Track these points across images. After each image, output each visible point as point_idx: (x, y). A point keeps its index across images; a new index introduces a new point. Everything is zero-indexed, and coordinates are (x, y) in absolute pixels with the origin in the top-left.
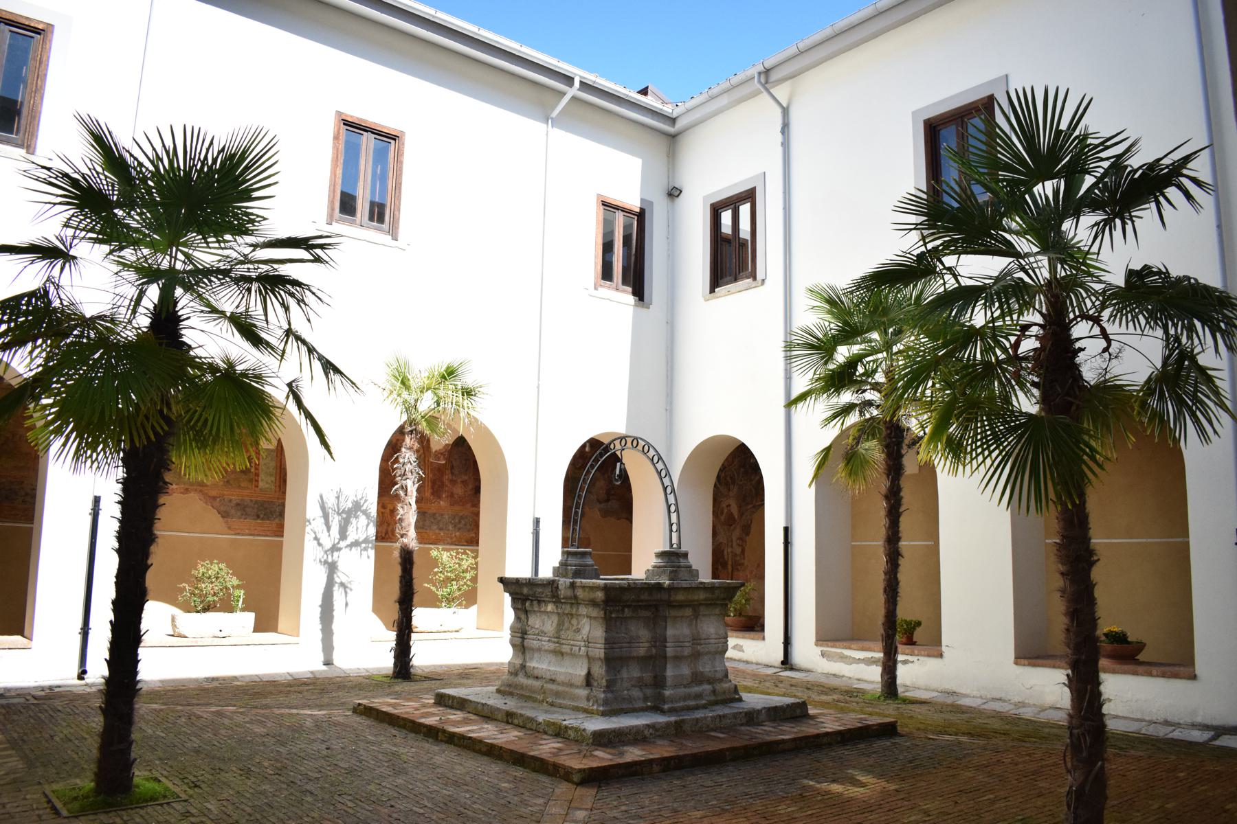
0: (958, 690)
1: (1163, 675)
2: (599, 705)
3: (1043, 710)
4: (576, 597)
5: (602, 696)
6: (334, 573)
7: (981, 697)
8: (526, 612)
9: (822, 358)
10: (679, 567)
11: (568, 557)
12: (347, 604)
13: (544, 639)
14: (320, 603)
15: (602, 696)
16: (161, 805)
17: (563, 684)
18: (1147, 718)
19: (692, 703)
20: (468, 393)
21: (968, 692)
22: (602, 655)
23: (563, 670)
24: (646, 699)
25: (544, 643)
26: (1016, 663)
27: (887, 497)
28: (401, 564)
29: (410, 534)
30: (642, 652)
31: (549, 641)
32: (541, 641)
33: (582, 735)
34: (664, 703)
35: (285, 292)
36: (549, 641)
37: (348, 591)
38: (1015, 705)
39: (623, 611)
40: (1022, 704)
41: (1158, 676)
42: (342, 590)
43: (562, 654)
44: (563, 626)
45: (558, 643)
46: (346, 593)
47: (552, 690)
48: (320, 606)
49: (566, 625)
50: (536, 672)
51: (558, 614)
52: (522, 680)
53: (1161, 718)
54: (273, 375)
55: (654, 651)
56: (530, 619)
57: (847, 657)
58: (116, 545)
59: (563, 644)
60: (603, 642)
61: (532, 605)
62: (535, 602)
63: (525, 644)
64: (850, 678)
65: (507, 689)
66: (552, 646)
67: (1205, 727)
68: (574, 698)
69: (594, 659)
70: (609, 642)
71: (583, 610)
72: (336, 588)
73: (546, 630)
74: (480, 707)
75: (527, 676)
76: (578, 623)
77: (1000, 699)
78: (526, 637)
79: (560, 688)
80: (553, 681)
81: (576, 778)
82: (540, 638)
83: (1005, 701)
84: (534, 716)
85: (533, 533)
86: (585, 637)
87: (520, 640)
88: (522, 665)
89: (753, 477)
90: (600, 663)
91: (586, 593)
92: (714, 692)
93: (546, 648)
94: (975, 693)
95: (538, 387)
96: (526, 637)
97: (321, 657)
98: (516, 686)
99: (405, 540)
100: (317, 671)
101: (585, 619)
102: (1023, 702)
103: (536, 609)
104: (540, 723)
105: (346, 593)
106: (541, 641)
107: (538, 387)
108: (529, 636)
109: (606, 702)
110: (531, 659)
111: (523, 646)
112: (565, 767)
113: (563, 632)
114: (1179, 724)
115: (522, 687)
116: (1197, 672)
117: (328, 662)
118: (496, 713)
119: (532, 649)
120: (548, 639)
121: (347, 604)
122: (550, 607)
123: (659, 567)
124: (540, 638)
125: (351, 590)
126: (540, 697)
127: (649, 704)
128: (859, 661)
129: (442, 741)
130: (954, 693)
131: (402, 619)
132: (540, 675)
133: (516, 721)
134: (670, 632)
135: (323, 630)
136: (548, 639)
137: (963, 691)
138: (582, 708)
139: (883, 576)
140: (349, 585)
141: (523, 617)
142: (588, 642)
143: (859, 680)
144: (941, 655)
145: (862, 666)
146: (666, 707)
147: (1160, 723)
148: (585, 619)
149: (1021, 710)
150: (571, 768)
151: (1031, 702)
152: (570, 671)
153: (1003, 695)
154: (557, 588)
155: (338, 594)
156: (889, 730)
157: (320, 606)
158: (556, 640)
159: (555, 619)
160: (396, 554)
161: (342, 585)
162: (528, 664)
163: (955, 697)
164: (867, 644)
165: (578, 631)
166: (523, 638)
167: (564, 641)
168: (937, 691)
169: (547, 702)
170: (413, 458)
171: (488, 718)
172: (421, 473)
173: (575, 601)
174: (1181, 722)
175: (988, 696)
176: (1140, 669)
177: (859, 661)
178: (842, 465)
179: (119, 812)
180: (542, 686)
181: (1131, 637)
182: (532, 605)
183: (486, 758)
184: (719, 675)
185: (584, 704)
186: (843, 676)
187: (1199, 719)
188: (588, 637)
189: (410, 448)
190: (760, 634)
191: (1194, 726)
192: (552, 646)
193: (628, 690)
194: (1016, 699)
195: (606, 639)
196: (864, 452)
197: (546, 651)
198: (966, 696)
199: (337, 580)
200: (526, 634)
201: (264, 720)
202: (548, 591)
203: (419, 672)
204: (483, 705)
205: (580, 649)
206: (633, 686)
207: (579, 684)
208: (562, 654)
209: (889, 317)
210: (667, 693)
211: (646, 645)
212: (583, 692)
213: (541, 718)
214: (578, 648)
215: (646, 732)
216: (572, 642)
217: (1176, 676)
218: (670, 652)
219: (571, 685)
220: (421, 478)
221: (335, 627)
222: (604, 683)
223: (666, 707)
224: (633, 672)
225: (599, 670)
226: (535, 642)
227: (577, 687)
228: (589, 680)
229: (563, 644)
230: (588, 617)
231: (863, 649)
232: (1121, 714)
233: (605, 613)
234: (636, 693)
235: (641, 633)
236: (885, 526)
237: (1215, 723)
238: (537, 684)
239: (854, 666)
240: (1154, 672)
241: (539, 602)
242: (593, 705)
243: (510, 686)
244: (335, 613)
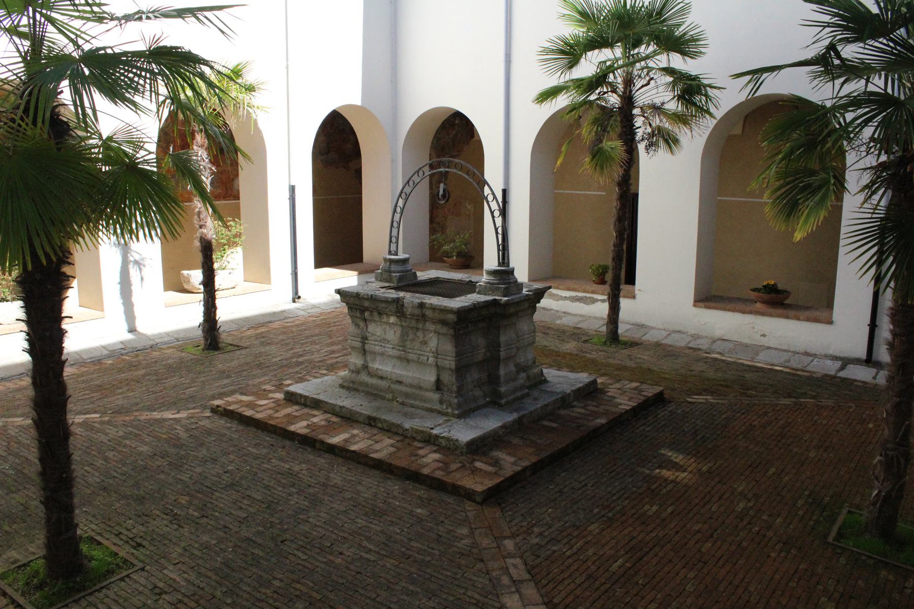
0: (646, 323)
1: (808, 320)
2: (453, 409)
3: (714, 341)
4: (424, 316)
5: (456, 401)
6: (128, 252)
7: (664, 329)
8: (365, 320)
9: (570, 62)
10: (510, 283)
11: (390, 264)
12: (142, 279)
13: (388, 346)
14: (118, 280)
15: (456, 401)
16: (122, 579)
17: (411, 386)
18: (792, 350)
19: (519, 394)
20: (250, 89)
21: (654, 325)
22: (453, 367)
23: (410, 374)
24: (485, 396)
25: (389, 350)
26: (695, 306)
27: (619, 184)
28: (202, 251)
29: (208, 224)
30: (480, 357)
31: (393, 348)
32: (384, 347)
33: (454, 444)
34: (501, 398)
35: (194, 75)
36: (393, 348)
37: (142, 267)
38: (692, 337)
39: (467, 326)
40: (696, 337)
41: (804, 320)
42: (136, 267)
43: (408, 361)
44: (408, 336)
45: (403, 351)
46: (140, 269)
47: (401, 391)
48: (119, 283)
49: (411, 336)
50: (380, 373)
51: (402, 326)
52: (364, 377)
53: (802, 350)
54: (148, 140)
55: (488, 354)
56: (369, 327)
57: (554, 295)
58: (26, 345)
59: (409, 352)
60: (454, 355)
61: (371, 315)
62: (375, 314)
63: (367, 347)
64: (557, 311)
65: (351, 385)
66: (395, 353)
67: (835, 358)
68: (425, 400)
69: (443, 368)
70: (459, 355)
71: (430, 326)
72: (131, 266)
73: (389, 339)
74: (337, 409)
75: (370, 374)
76: (424, 336)
77: (679, 332)
78: (366, 342)
79: (409, 390)
80: (400, 383)
81: (478, 499)
82: (383, 345)
83: (683, 333)
84: (399, 423)
85: (289, 199)
86: (434, 349)
87: (361, 344)
88: (363, 365)
89: (450, 131)
90: (450, 372)
91: (436, 314)
92: (528, 377)
93: (391, 353)
94: (660, 326)
95: (287, 68)
96: (366, 342)
97: (125, 327)
98: (361, 384)
99: (205, 231)
100: (126, 341)
101: (432, 334)
102: (697, 334)
103: (377, 319)
104: (407, 430)
105: (140, 269)
106: (384, 347)
107: (287, 68)
108: (370, 342)
109: (459, 406)
110: (374, 360)
111: (364, 350)
112: (464, 488)
113: (408, 343)
114: (815, 355)
115: (367, 385)
116: (834, 319)
117: (132, 330)
118: (356, 415)
119: (374, 353)
120: (391, 346)
121: (142, 279)
122: (392, 319)
123: (493, 284)
124: (383, 345)
125: (144, 266)
126: (389, 396)
127: (488, 399)
128: (565, 298)
129: (320, 449)
130: (642, 326)
131: (208, 300)
132: (384, 376)
133: (379, 425)
134: (503, 339)
135: (124, 304)
136: (391, 346)
137: (650, 324)
138: (436, 410)
139: (612, 248)
140: (142, 262)
141: (362, 324)
142: (437, 354)
143: (565, 313)
144: (634, 297)
145: (568, 302)
146: (503, 401)
147: (801, 354)
148: (432, 334)
149: (699, 341)
150: (473, 490)
151: (704, 334)
152: (417, 375)
153: (682, 329)
154: (403, 305)
155: (133, 272)
156: (659, 400)
157: (119, 283)
158: (401, 348)
159: (399, 331)
160: (197, 244)
161: (136, 262)
162: (370, 365)
163: (645, 329)
164: (569, 283)
165: (424, 343)
166: (364, 343)
167: (410, 351)
168: (630, 324)
169: (397, 401)
170: (205, 156)
171: (349, 419)
172: (213, 168)
173: (423, 318)
174: (817, 353)
175: (671, 329)
176: (791, 313)
177: (565, 298)
178: (587, 159)
179: (90, 599)
180: (389, 387)
181: (780, 287)
182: (371, 315)
183: (377, 472)
184: (530, 363)
185: (437, 407)
186: (551, 310)
187: (831, 352)
188: (437, 349)
189: (202, 146)
190: (478, 272)
191: (826, 356)
192: (395, 353)
193: (472, 391)
194: (693, 332)
195: (456, 353)
196: (609, 150)
197: (389, 356)
198: (653, 328)
199: (132, 259)
200: (367, 339)
201: (138, 432)
202: (393, 307)
203: (229, 340)
204: (341, 407)
205: (428, 359)
206: (475, 387)
207: (429, 388)
208: (408, 361)
209: (636, 31)
210: (503, 389)
211: (483, 350)
212: (436, 396)
213: (407, 424)
214: (426, 358)
215: (500, 432)
216: (419, 352)
217: (816, 320)
218: (503, 354)
219: (420, 388)
220: (213, 173)
221: (134, 299)
222: (455, 388)
223: (503, 401)
224: (474, 375)
225: (448, 378)
226: (377, 348)
227: (427, 390)
228: (438, 386)
229: (409, 352)
230: (435, 332)
231: (569, 289)
232: (772, 346)
233: (455, 331)
234: (478, 393)
235: (479, 341)
236: (616, 208)
237: (842, 355)
238: (383, 384)
239: (561, 302)
240: (802, 318)
241: (380, 314)
242: (447, 408)
243: (353, 382)
244: (133, 288)
